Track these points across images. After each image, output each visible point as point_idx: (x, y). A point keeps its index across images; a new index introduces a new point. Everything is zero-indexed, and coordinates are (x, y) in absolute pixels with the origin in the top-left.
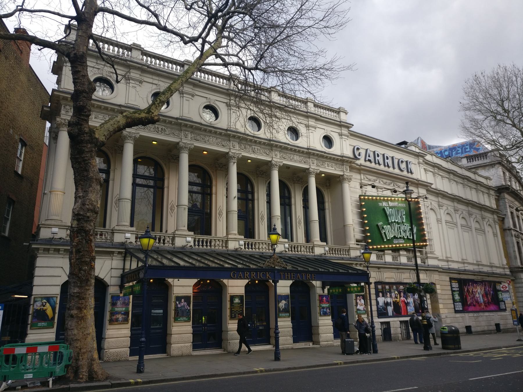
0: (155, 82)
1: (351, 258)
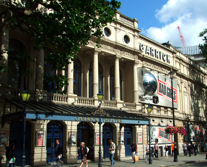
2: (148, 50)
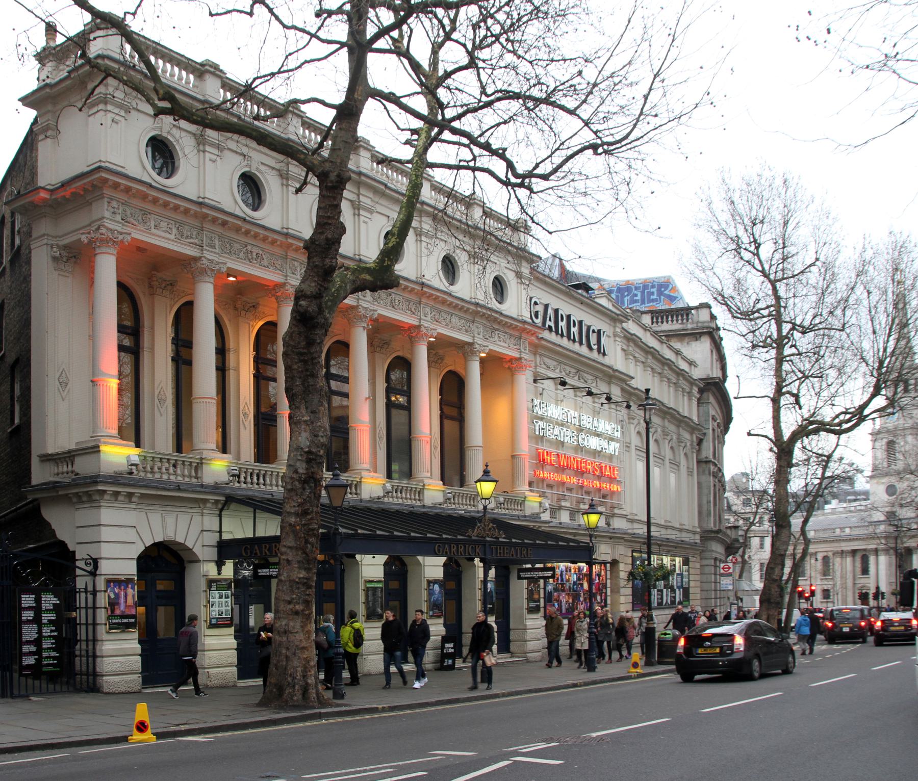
0: (245, 150)
1: (202, 486)
2: (550, 320)
